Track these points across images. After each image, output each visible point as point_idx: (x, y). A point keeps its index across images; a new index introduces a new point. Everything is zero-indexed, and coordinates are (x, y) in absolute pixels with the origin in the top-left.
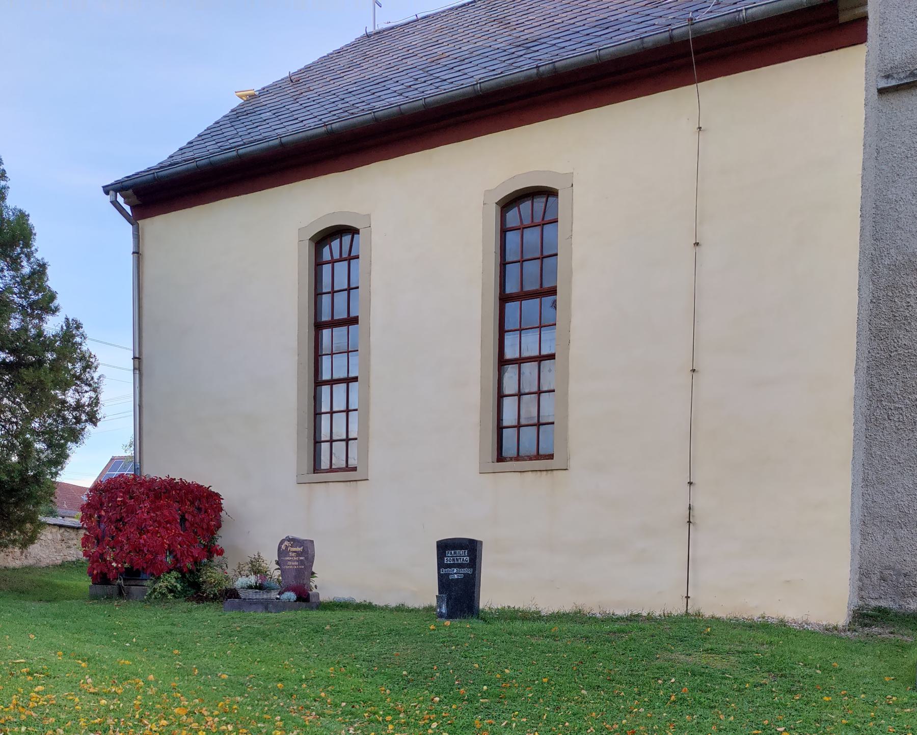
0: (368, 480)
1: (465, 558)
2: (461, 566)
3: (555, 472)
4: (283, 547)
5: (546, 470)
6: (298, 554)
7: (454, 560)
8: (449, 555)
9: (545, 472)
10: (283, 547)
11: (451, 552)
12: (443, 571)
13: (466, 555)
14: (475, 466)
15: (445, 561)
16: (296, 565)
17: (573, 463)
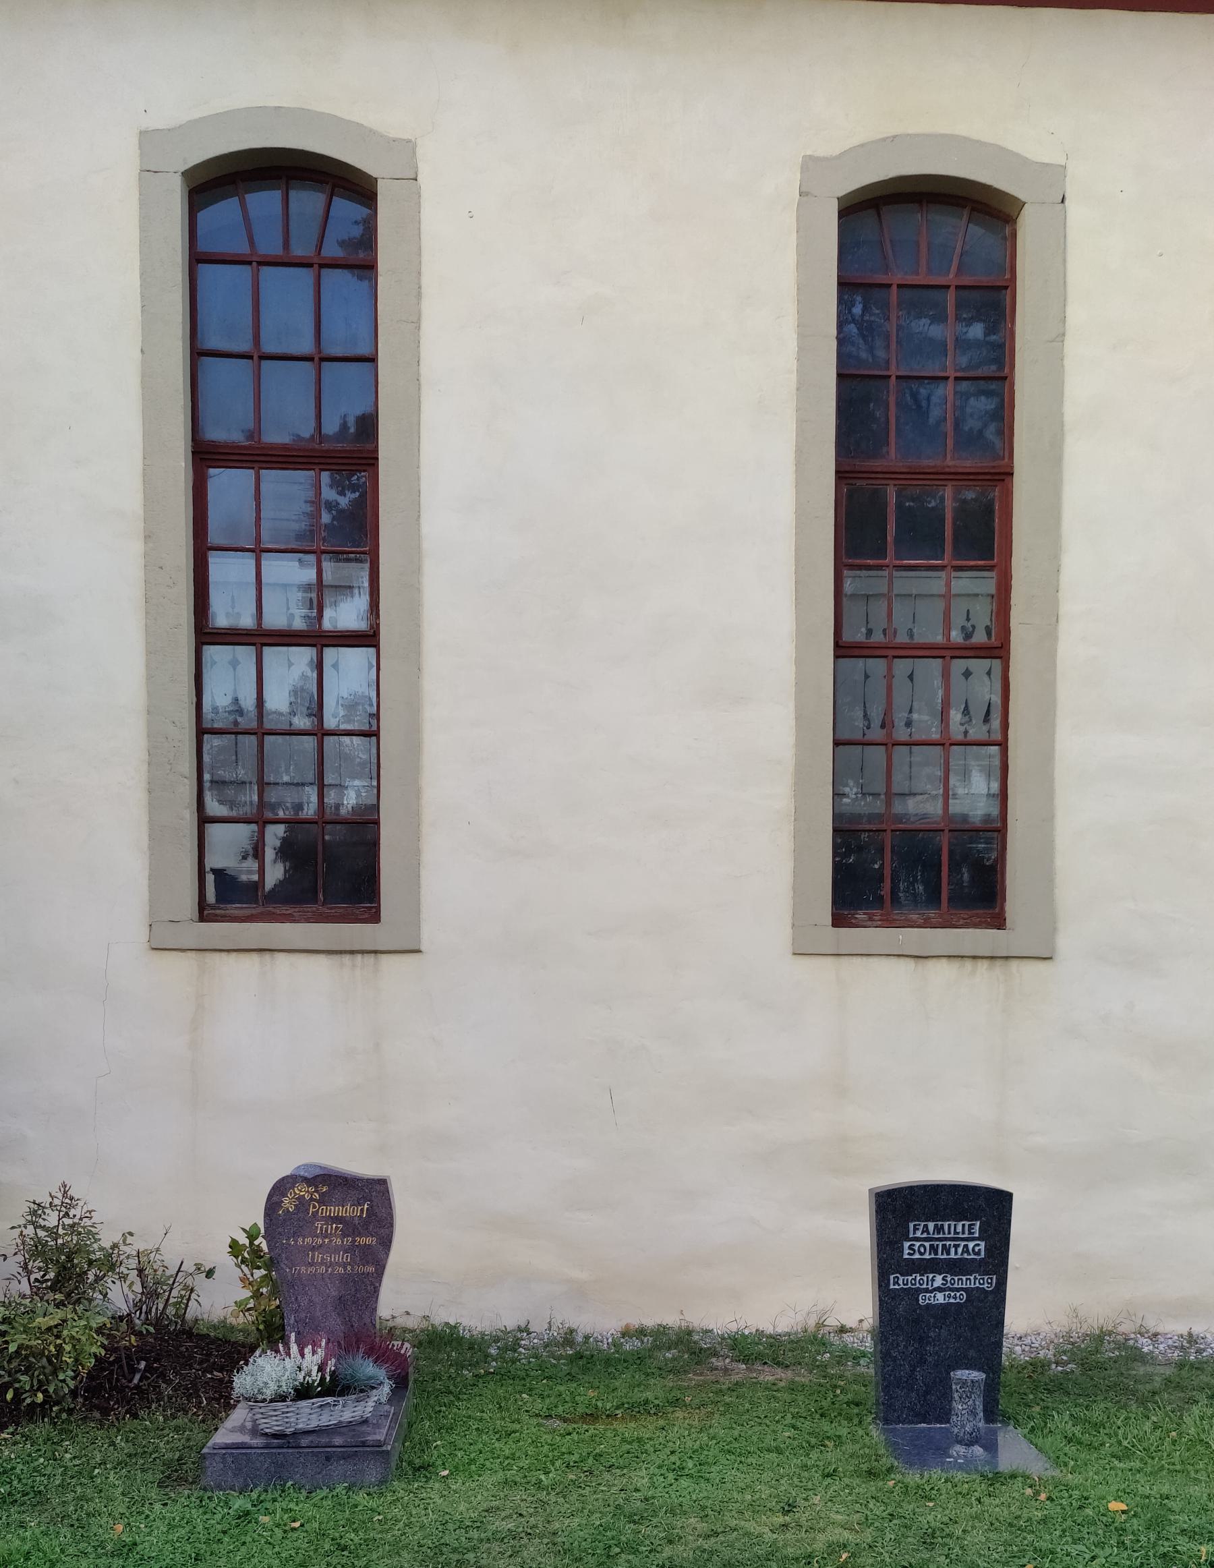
0: (419, 951)
1: (971, 1245)
2: (957, 1267)
3: (1014, 964)
4: (288, 1203)
5: (974, 957)
6: (350, 1227)
7: (934, 1249)
8: (918, 1234)
9: (986, 963)
10: (288, 1203)
11: (926, 1226)
12: (899, 1282)
13: (977, 1235)
14: (779, 932)
15: (906, 1251)
16: (345, 1266)
17: (1064, 943)
